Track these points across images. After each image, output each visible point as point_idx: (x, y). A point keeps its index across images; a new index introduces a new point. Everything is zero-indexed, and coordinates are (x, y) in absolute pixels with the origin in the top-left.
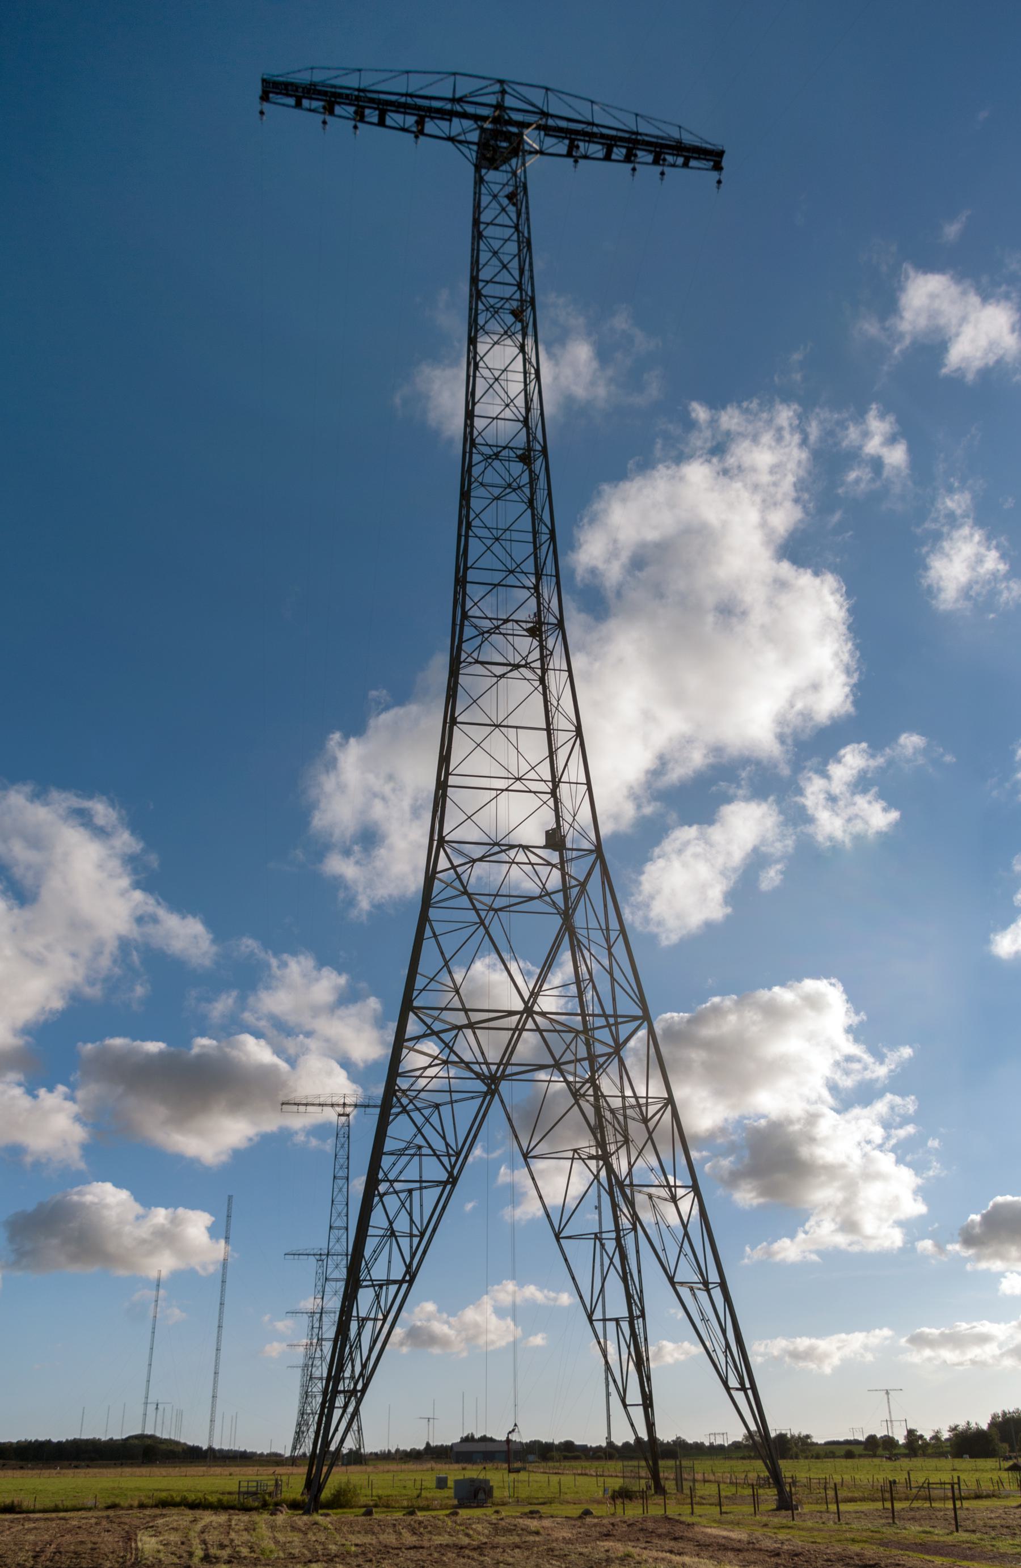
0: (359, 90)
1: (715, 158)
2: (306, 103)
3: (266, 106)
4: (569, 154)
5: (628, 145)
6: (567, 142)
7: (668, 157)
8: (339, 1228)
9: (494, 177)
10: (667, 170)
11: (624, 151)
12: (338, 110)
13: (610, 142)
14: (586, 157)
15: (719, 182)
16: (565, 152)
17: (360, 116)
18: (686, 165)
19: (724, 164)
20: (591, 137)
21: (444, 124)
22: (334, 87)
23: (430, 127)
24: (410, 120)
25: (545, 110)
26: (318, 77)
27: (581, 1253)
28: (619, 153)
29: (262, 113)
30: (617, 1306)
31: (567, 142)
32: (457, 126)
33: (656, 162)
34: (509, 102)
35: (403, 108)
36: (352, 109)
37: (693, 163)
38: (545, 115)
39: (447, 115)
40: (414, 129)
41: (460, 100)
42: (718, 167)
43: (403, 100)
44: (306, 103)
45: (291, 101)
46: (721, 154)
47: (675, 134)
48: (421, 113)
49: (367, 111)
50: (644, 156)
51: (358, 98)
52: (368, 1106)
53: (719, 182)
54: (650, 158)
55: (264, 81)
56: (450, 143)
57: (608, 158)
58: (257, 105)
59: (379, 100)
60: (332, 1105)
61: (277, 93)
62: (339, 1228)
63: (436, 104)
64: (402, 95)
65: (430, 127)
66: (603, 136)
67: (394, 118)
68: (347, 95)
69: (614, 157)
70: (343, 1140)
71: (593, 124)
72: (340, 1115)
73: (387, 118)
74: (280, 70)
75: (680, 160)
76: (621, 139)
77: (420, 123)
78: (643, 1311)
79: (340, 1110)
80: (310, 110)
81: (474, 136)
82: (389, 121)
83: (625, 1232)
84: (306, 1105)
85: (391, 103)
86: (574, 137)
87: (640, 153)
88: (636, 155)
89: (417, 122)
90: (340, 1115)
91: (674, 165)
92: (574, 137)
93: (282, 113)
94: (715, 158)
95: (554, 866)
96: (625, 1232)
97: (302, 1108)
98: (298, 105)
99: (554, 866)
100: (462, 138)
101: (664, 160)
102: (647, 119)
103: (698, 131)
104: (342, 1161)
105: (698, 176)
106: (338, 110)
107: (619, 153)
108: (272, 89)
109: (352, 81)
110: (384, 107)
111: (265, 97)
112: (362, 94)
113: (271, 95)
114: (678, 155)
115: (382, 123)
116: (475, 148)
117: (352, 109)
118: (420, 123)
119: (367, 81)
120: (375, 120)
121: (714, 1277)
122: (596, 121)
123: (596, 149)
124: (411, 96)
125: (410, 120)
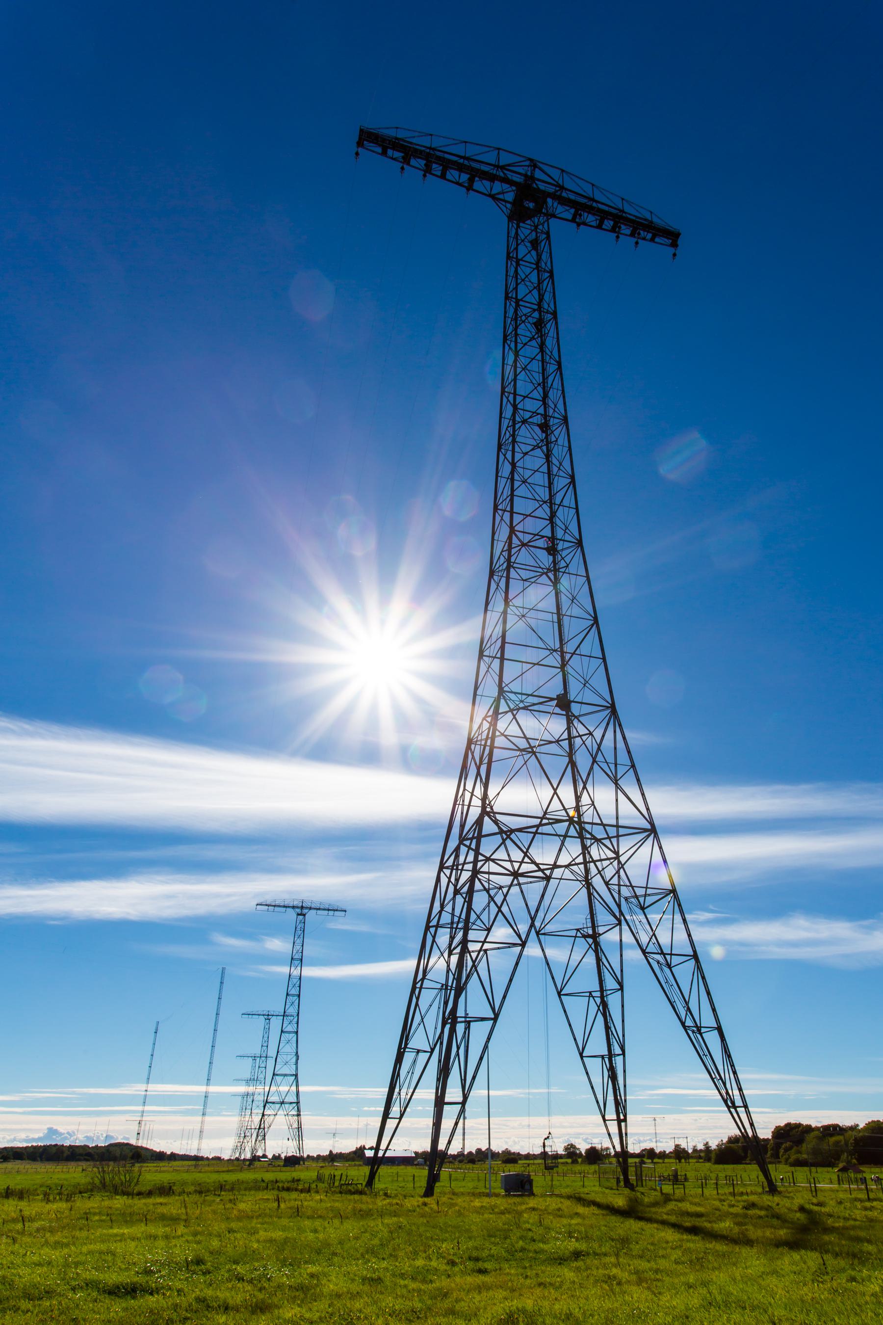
0: (430, 148)
1: (673, 237)
2: (390, 152)
3: (360, 150)
4: (573, 220)
5: (616, 220)
6: (573, 211)
7: (642, 232)
8: (293, 995)
9: (525, 230)
10: (640, 241)
11: (612, 223)
12: (413, 162)
13: (603, 215)
14: (585, 224)
15: (675, 255)
16: (570, 218)
17: (427, 170)
18: (652, 240)
19: (679, 242)
20: (590, 210)
21: (487, 183)
22: (411, 143)
23: (478, 185)
24: (465, 177)
25: (560, 182)
26: (401, 135)
27: (578, 1007)
28: (608, 224)
29: (357, 154)
30: (597, 1045)
31: (573, 211)
32: (498, 187)
33: (632, 235)
34: (538, 174)
35: (461, 168)
36: (423, 162)
37: (657, 240)
38: (562, 188)
39: (492, 178)
40: (466, 185)
41: (503, 168)
42: (674, 245)
43: (461, 161)
44: (390, 152)
45: (379, 150)
46: (678, 235)
47: (588, 190)
48: (471, 172)
49: (434, 166)
50: (626, 230)
51: (429, 154)
52: (319, 909)
53: (675, 255)
54: (628, 232)
55: (361, 131)
56: (490, 199)
57: (599, 227)
58: (354, 148)
59: (444, 158)
60: (293, 907)
61: (370, 142)
62: (293, 995)
63: (484, 168)
64: (461, 157)
65: (478, 185)
66: (599, 210)
67: (452, 174)
68: (421, 152)
69: (604, 227)
70: (300, 932)
71: (593, 200)
72: (298, 914)
73: (448, 173)
74: (370, 124)
75: (649, 236)
76: (610, 214)
77: (471, 181)
78: (623, 1048)
79: (299, 911)
80: (392, 158)
81: (510, 197)
82: (449, 176)
83: (609, 992)
84: (275, 906)
85: (454, 163)
86: (582, 208)
87: (623, 227)
88: (620, 228)
89: (469, 179)
90: (298, 914)
91: (644, 239)
92: (582, 208)
93: (371, 156)
94: (673, 237)
95: (502, 734)
96: (609, 992)
97: (331, 913)
98: (384, 153)
99: (502, 734)
100: (501, 197)
101: (639, 234)
102: (630, 203)
103: (665, 218)
104: (266, 1039)
105: (659, 250)
106: (413, 162)
107: (608, 224)
108: (366, 137)
109: (425, 142)
110: (446, 165)
111: (360, 144)
112: (432, 152)
113: (365, 142)
114: (648, 232)
115: (443, 176)
116: (509, 206)
117: (423, 162)
118: (471, 181)
119: (437, 143)
120: (439, 173)
121: (708, 1020)
122: (596, 198)
123: (591, 219)
124: (468, 159)
125: (465, 177)
